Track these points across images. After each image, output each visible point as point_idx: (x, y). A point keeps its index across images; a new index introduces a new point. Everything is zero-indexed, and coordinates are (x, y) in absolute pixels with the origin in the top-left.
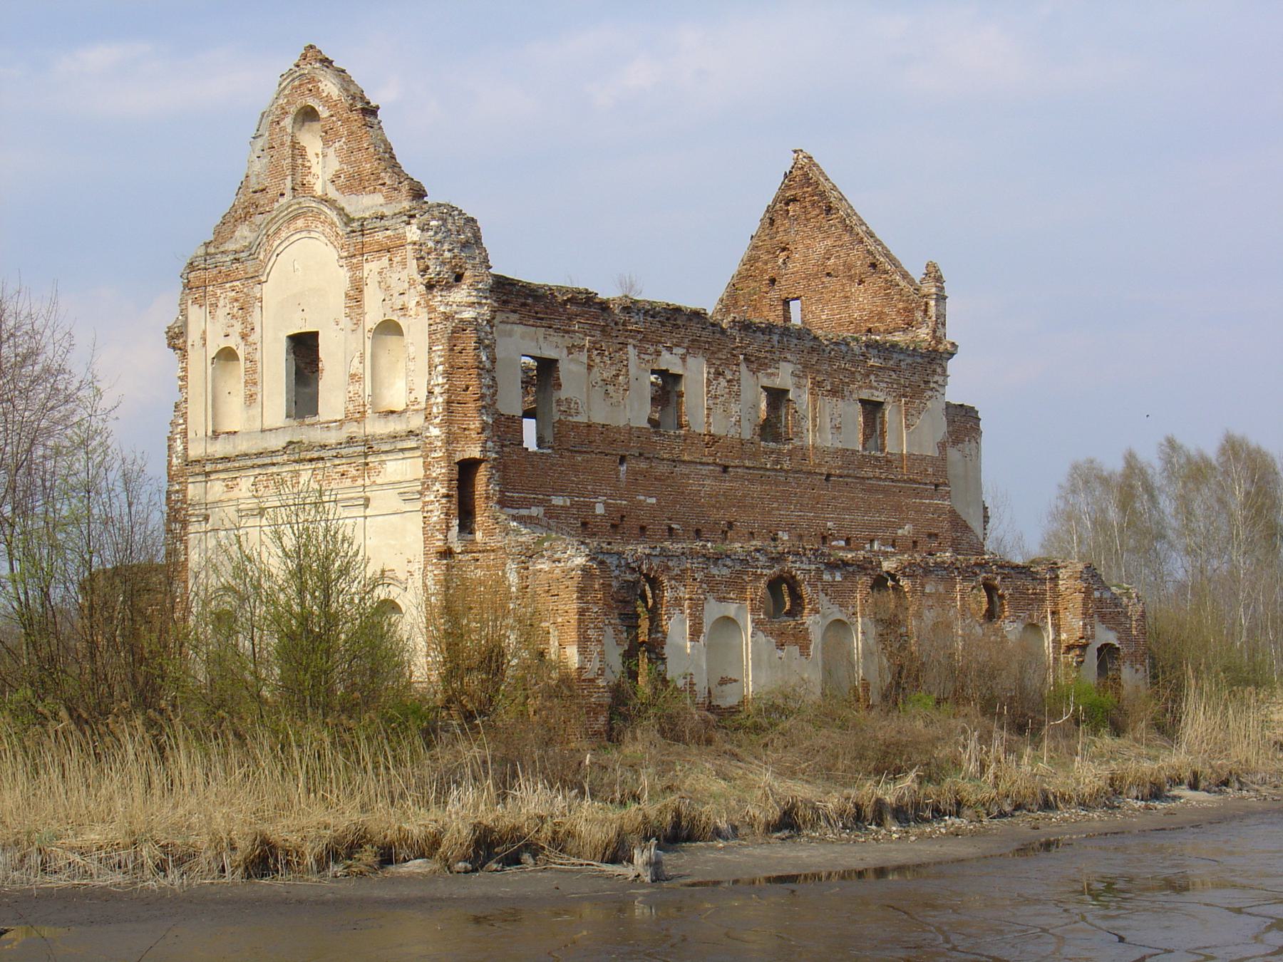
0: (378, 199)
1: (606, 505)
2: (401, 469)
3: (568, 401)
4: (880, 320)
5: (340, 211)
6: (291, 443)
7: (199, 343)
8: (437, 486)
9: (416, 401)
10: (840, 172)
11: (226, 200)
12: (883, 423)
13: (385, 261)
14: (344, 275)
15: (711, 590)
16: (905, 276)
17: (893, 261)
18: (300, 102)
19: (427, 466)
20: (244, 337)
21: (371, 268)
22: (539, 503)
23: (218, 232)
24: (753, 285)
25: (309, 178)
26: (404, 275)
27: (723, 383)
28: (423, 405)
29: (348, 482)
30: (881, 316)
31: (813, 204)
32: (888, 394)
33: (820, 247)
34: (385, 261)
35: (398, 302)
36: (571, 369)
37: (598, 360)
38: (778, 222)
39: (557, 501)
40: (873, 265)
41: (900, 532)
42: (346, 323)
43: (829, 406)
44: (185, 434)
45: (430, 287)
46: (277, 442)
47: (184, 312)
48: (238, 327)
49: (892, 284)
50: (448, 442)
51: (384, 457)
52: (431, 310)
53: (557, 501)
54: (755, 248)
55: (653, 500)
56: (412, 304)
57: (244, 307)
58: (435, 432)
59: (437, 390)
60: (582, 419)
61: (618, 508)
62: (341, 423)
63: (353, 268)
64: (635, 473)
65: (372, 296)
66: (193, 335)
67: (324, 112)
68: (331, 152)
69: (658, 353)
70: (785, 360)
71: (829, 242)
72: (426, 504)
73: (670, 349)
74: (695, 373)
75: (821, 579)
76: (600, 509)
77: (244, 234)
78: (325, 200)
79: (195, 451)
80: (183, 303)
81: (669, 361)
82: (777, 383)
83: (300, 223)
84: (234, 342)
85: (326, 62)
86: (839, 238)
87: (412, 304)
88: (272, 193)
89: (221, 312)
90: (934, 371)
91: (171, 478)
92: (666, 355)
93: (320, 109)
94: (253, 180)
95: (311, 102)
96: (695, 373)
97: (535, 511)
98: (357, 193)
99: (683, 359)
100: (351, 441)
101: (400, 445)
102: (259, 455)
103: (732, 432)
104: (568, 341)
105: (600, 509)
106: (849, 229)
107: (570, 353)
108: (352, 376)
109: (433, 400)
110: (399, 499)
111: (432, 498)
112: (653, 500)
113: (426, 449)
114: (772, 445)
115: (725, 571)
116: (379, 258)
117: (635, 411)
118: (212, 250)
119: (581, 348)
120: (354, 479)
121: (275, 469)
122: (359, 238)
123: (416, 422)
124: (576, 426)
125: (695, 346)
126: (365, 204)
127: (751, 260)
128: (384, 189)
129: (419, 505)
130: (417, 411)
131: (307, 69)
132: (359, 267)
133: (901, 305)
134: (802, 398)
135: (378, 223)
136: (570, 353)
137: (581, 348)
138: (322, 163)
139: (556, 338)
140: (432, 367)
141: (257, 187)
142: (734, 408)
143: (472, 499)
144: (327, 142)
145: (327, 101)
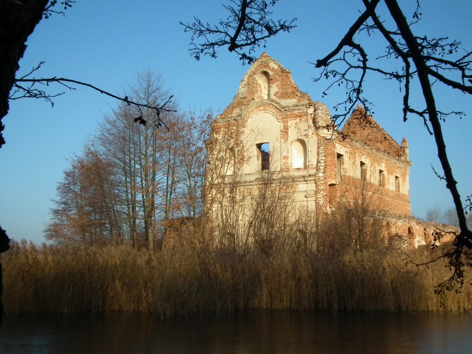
21: (291, 123)
25: (262, 94)
28: (315, 166)
38: (351, 125)
40: (385, 138)
49: (391, 144)
50: (325, 178)
51: (297, 183)
52: (318, 135)
56: (310, 134)
58: (321, 175)
60: (348, 174)
63: (284, 122)
77: (236, 111)
81: (363, 160)
83: (262, 108)
87: (310, 134)
98: (285, 98)
108: (284, 157)
109: (320, 165)
111: (321, 196)
116: (295, 119)
121: (251, 187)
122: (284, 113)
124: (347, 177)
128: (297, 97)
129: (314, 199)
130: (312, 168)
132: (287, 122)
133: (395, 150)
134: (385, 173)
141: (242, 97)
145: (273, 70)
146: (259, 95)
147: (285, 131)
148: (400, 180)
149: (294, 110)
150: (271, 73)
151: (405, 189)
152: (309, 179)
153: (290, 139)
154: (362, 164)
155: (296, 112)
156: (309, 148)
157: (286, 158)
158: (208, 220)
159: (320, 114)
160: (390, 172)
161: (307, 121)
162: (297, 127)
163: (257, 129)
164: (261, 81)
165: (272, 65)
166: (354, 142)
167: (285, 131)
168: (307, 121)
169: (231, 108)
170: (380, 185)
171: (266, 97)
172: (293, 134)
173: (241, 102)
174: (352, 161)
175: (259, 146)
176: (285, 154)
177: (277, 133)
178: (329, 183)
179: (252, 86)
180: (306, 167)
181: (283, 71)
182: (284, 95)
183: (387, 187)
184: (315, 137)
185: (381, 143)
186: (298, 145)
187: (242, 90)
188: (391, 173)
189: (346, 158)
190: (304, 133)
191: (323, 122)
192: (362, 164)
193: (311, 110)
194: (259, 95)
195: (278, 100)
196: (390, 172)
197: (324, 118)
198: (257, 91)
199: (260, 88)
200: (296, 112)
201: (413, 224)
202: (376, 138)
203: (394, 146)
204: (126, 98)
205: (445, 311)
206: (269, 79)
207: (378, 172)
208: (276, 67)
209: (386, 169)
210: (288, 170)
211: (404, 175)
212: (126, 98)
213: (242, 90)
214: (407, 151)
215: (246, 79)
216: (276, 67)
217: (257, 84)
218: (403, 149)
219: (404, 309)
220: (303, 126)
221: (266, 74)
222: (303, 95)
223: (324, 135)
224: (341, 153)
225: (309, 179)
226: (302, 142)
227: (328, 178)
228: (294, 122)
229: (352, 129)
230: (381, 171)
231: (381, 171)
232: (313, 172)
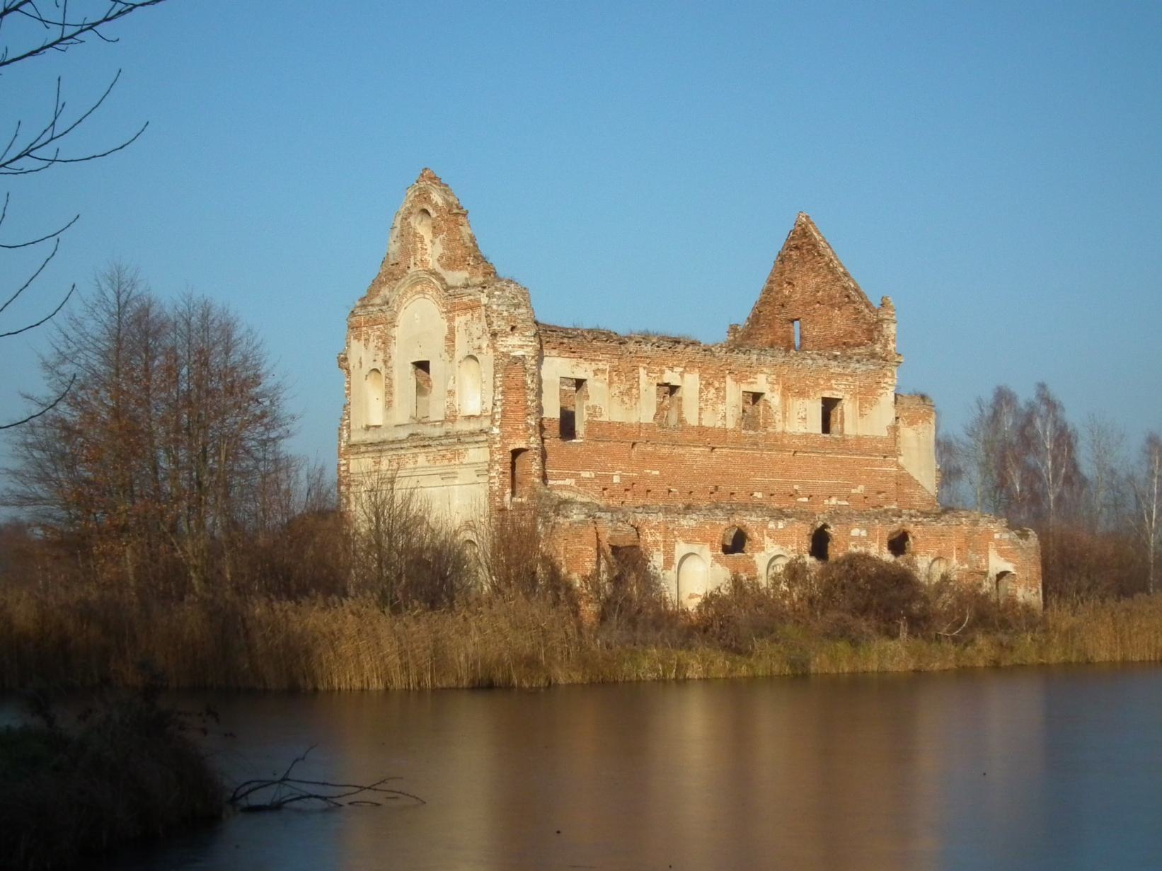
0: (465, 274)
1: (621, 476)
2: (477, 454)
3: (594, 407)
4: (852, 337)
5: (442, 280)
6: (412, 435)
7: (358, 365)
8: (497, 467)
9: (486, 410)
10: (826, 232)
11: (374, 271)
12: (842, 414)
13: (469, 316)
14: (445, 323)
15: (681, 535)
16: (868, 305)
17: (860, 294)
18: (420, 206)
19: (491, 453)
20: (385, 362)
21: (460, 320)
22: (572, 476)
23: (369, 291)
24: (769, 309)
26: (480, 327)
27: (712, 390)
29: (446, 462)
30: (852, 334)
31: (808, 251)
32: (847, 392)
33: (813, 282)
34: (469, 316)
35: (477, 343)
36: (596, 386)
37: (616, 379)
39: (585, 474)
41: (853, 491)
42: (446, 356)
43: (797, 405)
44: (349, 426)
45: (494, 335)
46: (403, 434)
47: (348, 344)
48: (381, 355)
49: (857, 311)
52: (495, 350)
53: (585, 474)
54: (771, 282)
55: (657, 473)
56: (484, 346)
57: (386, 341)
58: (496, 431)
59: (499, 403)
60: (604, 419)
61: (630, 478)
62: (442, 422)
64: (643, 453)
65: (460, 339)
66: (353, 362)
67: (434, 215)
68: (437, 241)
69: (662, 372)
70: (762, 372)
71: (818, 279)
72: (491, 478)
73: (671, 369)
74: (690, 384)
75: (766, 527)
76: (616, 479)
77: (385, 291)
78: (433, 273)
79: (354, 439)
80: (348, 337)
81: (671, 377)
82: (755, 389)
83: (419, 288)
84: (379, 365)
85: (434, 179)
86: (825, 277)
87: (484, 346)
88: (402, 266)
89: (372, 345)
90: (885, 375)
91: (340, 455)
92: (668, 372)
93: (431, 211)
94: (391, 257)
95: (426, 207)
96: (690, 384)
97: (568, 482)
98: (453, 269)
99: (682, 375)
100: (447, 435)
101: (477, 439)
102: (393, 442)
103: (719, 424)
104: (594, 366)
105: (616, 479)
106: (832, 271)
107: (596, 375)
108: (450, 391)
110: (474, 474)
112: (657, 473)
113: (491, 443)
114: (751, 432)
115: (693, 523)
117: (645, 412)
118: (366, 302)
119: (603, 371)
120: (450, 460)
121: (403, 452)
122: (453, 301)
123: (486, 424)
124: (600, 423)
125: (690, 365)
126: (456, 277)
127: (768, 291)
131: (422, 184)
133: (865, 326)
134: (774, 398)
135: (464, 291)
136: (596, 375)
137: (603, 371)
138: (432, 251)
139: (586, 365)
140: (495, 387)
142: (720, 407)
143: (832, 419)
144: (435, 234)
145: (435, 206)
146: (419, 258)
147: (451, 339)
149: (462, 295)
152: (468, 440)
155: (466, 299)
159: (495, 307)
164: (422, 228)
166: (632, 346)
167: (451, 339)
169: (378, 283)
173: (391, 273)
177: (441, 343)
178: (511, 448)
179: (408, 239)
185: (840, 309)
188: (802, 394)
191: (503, 323)
194: (419, 258)
197: (505, 314)
198: (415, 251)
199: (422, 242)
200: (466, 299)
201: (750, 521)
202: (831, 297)
203: (864, 317)
205: (387, 689)
209: (778, 388)
215: (398, 224)
217: (415, 234)
219: (553, 681)
223: (505, 350)
225: (468, 440)
227: (510, 436)
229: (787, 274)
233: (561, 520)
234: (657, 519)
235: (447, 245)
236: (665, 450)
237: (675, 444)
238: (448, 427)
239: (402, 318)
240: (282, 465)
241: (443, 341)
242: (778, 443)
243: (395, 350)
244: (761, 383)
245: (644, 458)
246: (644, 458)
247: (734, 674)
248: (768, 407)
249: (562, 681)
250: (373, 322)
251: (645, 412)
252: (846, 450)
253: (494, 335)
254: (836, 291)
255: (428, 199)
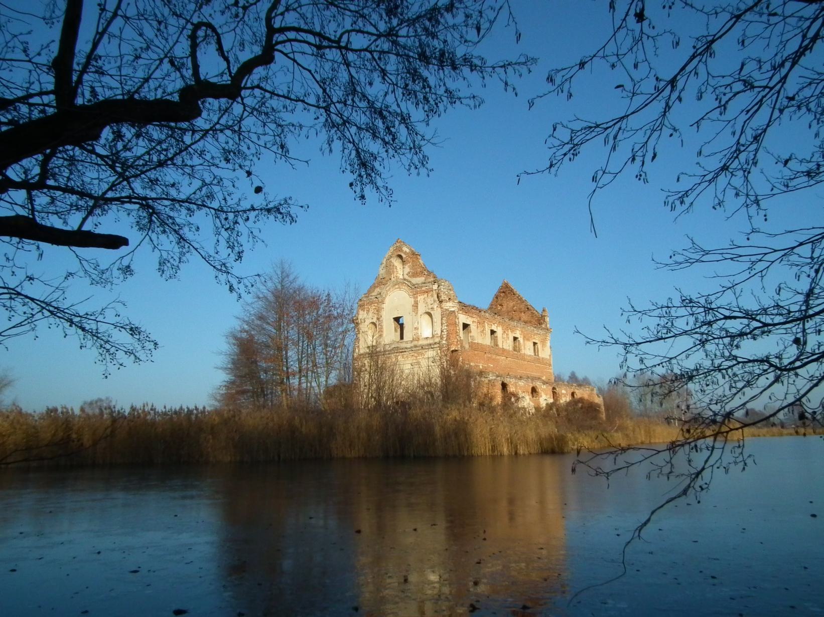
11: (372, 281)
21: (420, 298)
33: (511, 304)
45: (441, 302)
49: (533, 313)
52: (441, 308)
57: (378, 310)
77: (378, 290)
81: (494, 328)
106: (521, 299)
122: (415, 290)
134: (521, 339)
145: (405, 253)
147: (416, 306)
148: (539, 346)
150: (404, 256)
151: (545, 353)
153: (420, 312)
154: (493, 332)
156: (435, 320)
157: (416, 329)
158: (356, 386)
160: (526, 338)
161: (432, 296)
162: (426, 302)
163: (753, 272)
164: (397, 263)
165: (405, 249)
166: (483, 313)
167: (416, 306)
168: (432, 296)
169: (373, 287)
170: (515, 350)
171: (401, 277)
172: (422, 308)
173: (381, 282)
174: (480, 329)
175: (397, 319)
176: (416, 325)
177: (409, 307)
179: (389, 268)
180: (433, 336)
181: (413, 254)
182: (415, 275)
183: (523, 352)
184: (439, 309)
186: (427, 317)
187: (382, 271)
188: (528, 340)
189: (473, 327)
190: (430, 307)
192: (493, 332)
193: (435, 287)
195: (409, 279)
196: (526, 338)
201: (538, 384)
204: (252, 207)
206: (404, 262)
207: (511, 339)
208: (408, 251)
210: (418, 339)
211: (543, 342)
212: (252, 207)
213: (382, 271)
214: (547, 319)
216: (408, 251)
218: (543, 317)
220: (430, 300)
221: (400, 256)
222: (429, 273)
224: (468, 323)
226: (430, 314)
228: (422, 297)
230: (515, 339)
231: (515, 339)
232: (437, 340)
233: (483, 379)
234: (513, 381)
235: (413, 267)
236: (494, 357)
237: (497, 355)
238: (415, 343)
239: (387, 300)
240: (217, 412)
241: (411, 307)
242: (523, 358)
243: (384, 313)
244: (518, 334)
245: (489, 359)
246: (489, 358)
247: (819, 417)
248: (519, 343)
249: (522, 452)
250: (372, 303)
251: (487, 341)
252: (540, 363)
253: (441, 302)
254: (522, 306)
255: (401, 250)
